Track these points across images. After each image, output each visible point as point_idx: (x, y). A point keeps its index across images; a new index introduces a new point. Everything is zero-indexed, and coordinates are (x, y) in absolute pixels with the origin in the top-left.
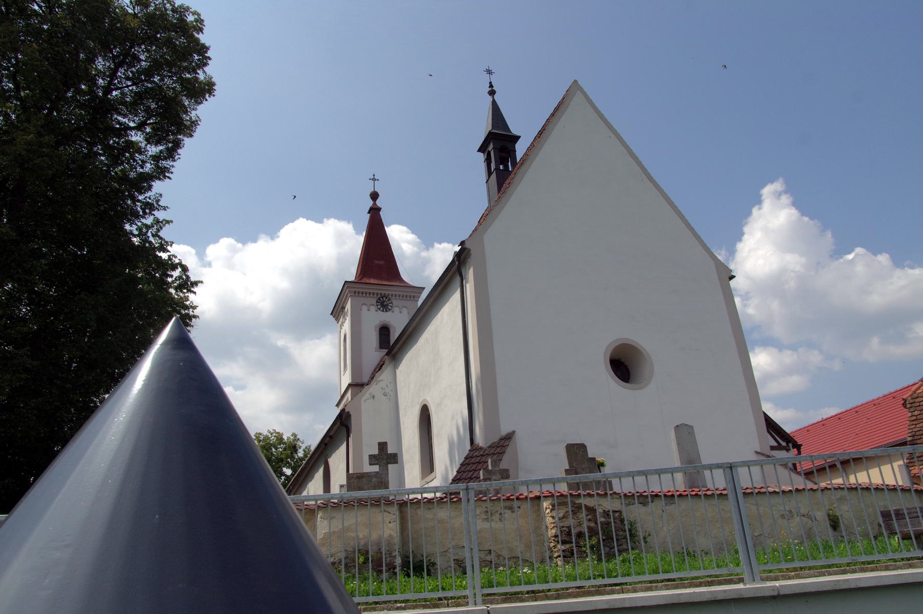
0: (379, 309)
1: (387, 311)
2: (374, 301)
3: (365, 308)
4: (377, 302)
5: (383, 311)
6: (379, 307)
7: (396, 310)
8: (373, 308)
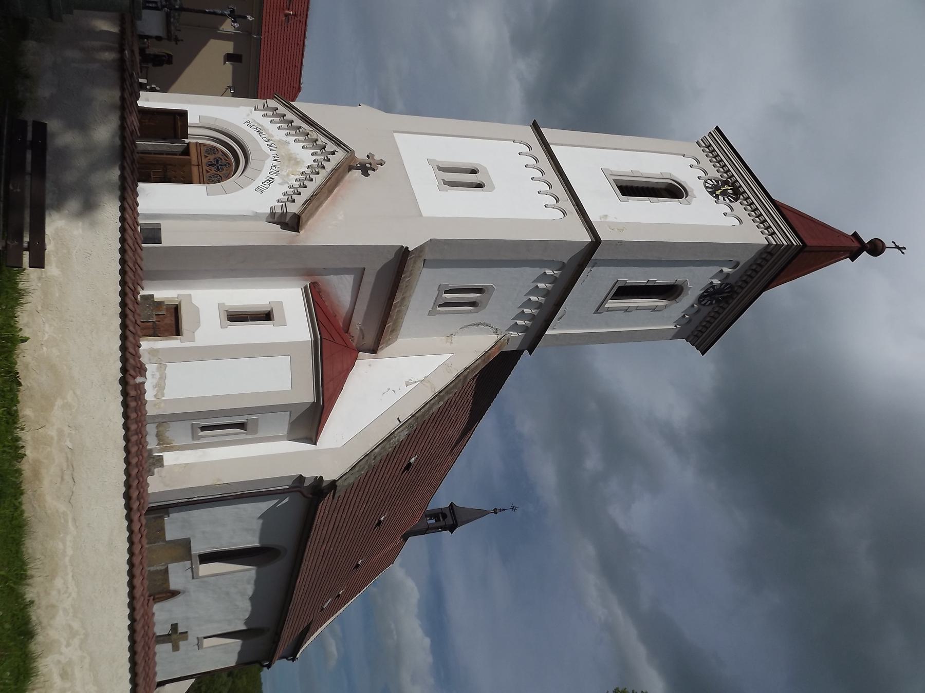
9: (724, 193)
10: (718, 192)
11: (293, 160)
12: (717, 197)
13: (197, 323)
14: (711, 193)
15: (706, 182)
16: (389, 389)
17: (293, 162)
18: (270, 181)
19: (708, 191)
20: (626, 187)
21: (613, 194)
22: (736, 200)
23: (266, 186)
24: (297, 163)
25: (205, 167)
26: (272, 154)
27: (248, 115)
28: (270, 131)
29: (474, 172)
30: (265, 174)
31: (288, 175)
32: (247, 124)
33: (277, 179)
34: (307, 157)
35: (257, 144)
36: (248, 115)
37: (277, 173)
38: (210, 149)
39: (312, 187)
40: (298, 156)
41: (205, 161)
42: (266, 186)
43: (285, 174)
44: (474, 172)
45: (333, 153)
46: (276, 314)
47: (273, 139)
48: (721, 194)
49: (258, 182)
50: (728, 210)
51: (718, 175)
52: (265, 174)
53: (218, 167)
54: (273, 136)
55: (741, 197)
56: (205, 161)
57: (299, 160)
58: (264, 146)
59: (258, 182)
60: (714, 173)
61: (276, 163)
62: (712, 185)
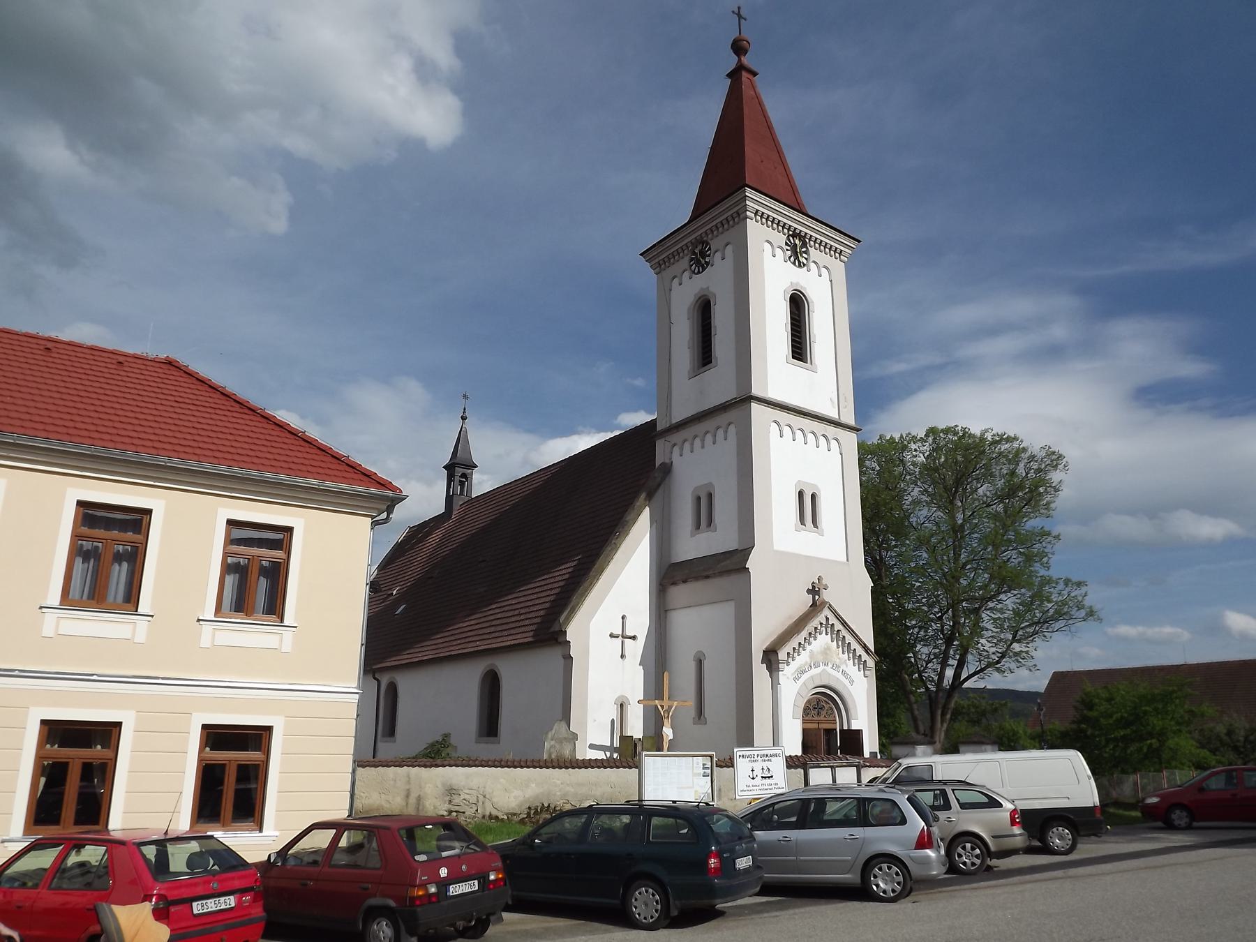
4: (692, 259)
9: (703, 254)
10: (703, 262)
11: (826, 651)
12: (707, 263)
14: (704, 269)
15: (694, 272)
17: (828, 652)
18: (844, 673)
19: (702, 272)
20: (704, 359)
21: (710, 374)
22: (708, 244)
24: (828, 648)
25: (822, 718)
26: (822, 667)
27: (788, 678)
28: (803, 663)
29: (699, 499)
30: (839, 675)
31: (839, 659)
33: (843, 667)
34: (823, 640)
35: (817, 675)
36: (788, 678)
37: (838, 667)
39: (794, 643)
43: (838, 660)
44: (699, 499)
45: (827, 619)
47: (809, 662)
48: (704, 258)
49: (846, 682)
50: (718, 255)
51: (687, 259)
52: (839, 675)
54: (807, 662)
55: (705, 239)
56: (816, 718)
58: (815, 671)
59: (846, 682)
60: (685, 262)
61: (830, 665)
62: (696, 266)
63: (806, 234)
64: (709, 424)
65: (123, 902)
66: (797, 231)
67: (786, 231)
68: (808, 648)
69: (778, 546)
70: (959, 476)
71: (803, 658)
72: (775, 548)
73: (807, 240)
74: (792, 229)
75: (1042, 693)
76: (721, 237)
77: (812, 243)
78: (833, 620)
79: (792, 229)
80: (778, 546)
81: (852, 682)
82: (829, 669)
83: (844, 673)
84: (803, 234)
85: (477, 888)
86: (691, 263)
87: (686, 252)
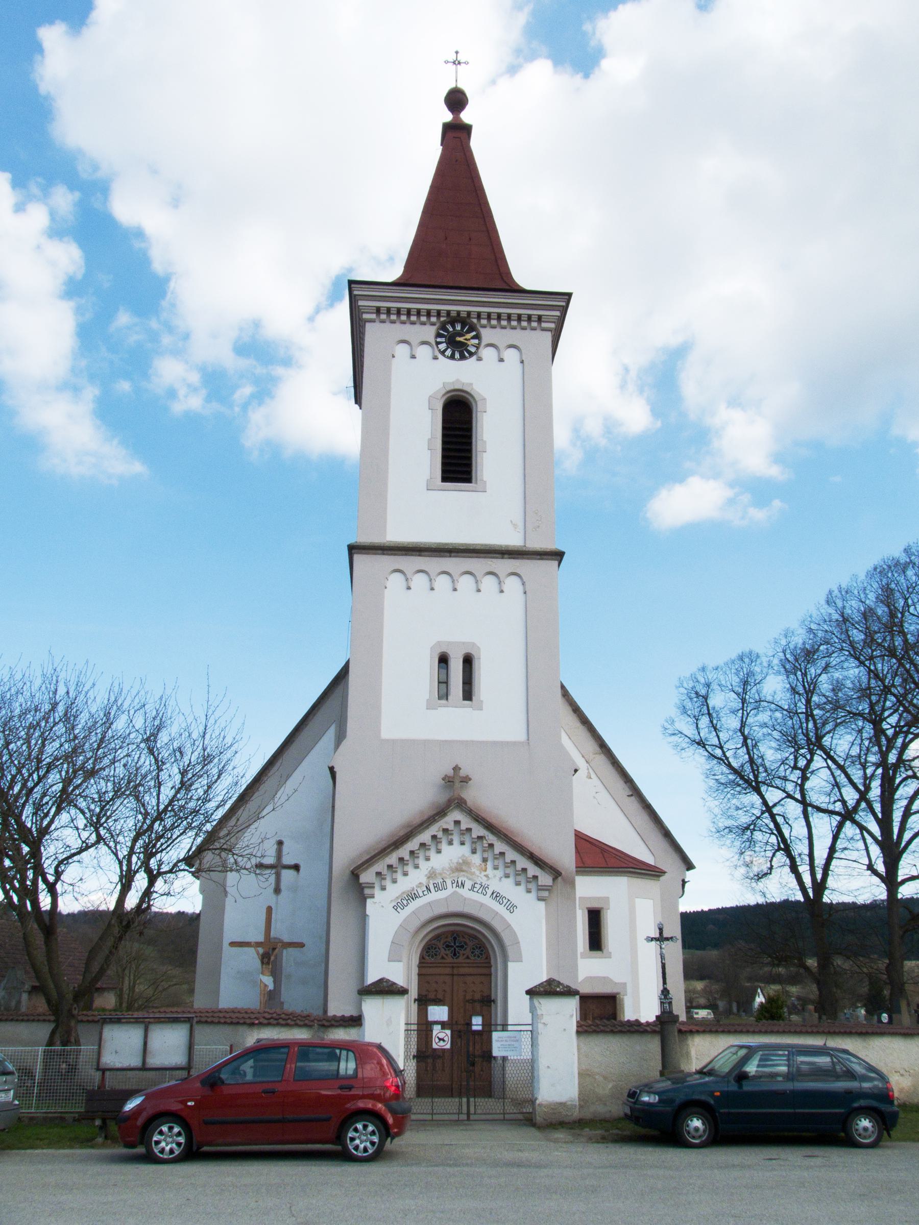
0: (443, 353)
1: (463, 357)
2: (429, 332)
3: (402, 351)
4: (438, 335)
5: (452, 357)
6: (443, 347)
7: (488, 354)
8: (424, 352)
13: (605, 980)
16: (594, 797)
18: (496, 896)
23: (505, 901)
25: (461, 959)
30: (487, 901)
32: (399, 909)
38: (427, 952)
40: (455, 861)
41: (449, 960)
42: (505, 901)
46: (595, 905)
52: (487, 901)
53: (458, 947)
57: (461, 861)
58: (434, 896)
63: (469, 313)
64: (478, 565)
65: (577, 978)
66: (453, 314)
67: (433, 319)
68: (424, 866)
69: (389, 730)
70: (803, 671)
71: (415, 878)
72: (386, 734)
73: (475, 321)
74: (443, 314)
75: (39, 25)
76: (518, 332)
77: (484, 322)
78: (466, 822)
79: (443, 314)
80: (389, 730)
81: (511, 908)
82: (465, 892)
83: (496, 896)
84: (464, 315)
85: (435, 1046)
86: (439, 340)
87: (433, 319)
